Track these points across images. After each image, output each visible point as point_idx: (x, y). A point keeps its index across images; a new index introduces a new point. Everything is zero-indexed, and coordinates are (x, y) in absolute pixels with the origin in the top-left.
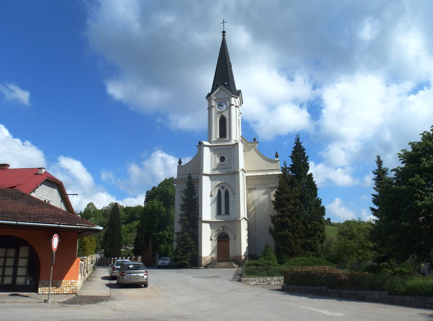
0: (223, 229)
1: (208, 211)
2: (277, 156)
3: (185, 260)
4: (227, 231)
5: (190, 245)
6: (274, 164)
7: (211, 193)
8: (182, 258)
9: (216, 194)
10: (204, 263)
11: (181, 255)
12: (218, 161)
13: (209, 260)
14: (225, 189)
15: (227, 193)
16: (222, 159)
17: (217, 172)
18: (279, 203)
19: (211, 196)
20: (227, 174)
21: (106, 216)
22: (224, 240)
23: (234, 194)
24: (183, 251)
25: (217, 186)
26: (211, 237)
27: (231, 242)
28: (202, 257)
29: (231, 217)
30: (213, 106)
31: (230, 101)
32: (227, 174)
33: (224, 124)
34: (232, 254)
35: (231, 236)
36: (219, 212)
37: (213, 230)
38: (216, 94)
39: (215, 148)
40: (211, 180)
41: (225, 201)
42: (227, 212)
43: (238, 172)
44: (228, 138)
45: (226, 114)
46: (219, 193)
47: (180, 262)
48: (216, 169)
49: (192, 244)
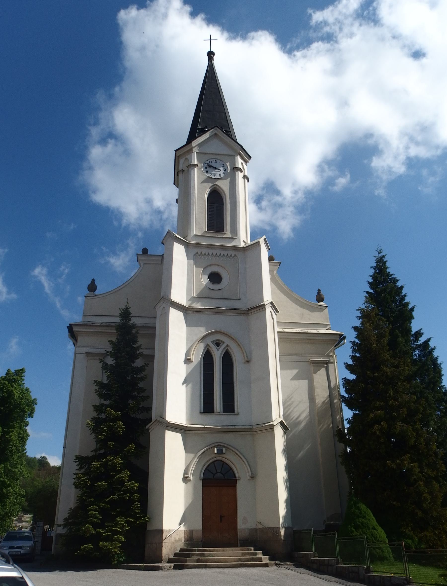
0: (220, 451)
1: (177, 402)
2: (320, 298)
3: (107, 539)
4: (230, 458)
5: (125, 492)
6: (317, 314)
7: (188, 353)
8: (99, 534)
9: (197, 357)
10: (167, 550)
11: (95, 526)
12: (205, 280)
13: (179, 540)
14: (222, 347)
15: (227, 359)
16: (215, 278)
17: (197, 305)
18: (358, 393)
19: (188, 360)
20: (228, 311)
21: (187, 158)
22: (217, 483)
23: (248, 361)
24: (102, 511)
25: (203, 339)
26: (186, 472)
27: (242, 489)
28: (161, 531)
29: (240, 419)
30: (196, 166)
31: (233, 162)
32: (228, 311)
33: (218, 208)
34: (245, 521)
35: (241, 471)
36: (208, 407)
37: (192, 455)
38: (200, 145)
39: (199, 250)
40: (189, 323)
41: (221, 380)
42: (229, 407)
43: (264, 305)
44: (229, 235)
45: (224, 185)
46: (207, 358)
47: (90, 546)
48: (199, 297)
49: (131, 491)
